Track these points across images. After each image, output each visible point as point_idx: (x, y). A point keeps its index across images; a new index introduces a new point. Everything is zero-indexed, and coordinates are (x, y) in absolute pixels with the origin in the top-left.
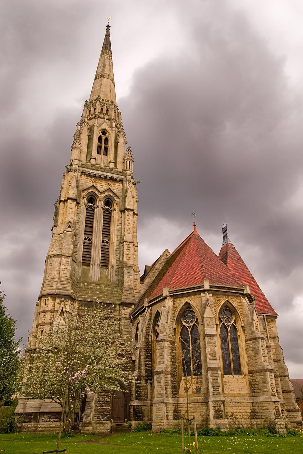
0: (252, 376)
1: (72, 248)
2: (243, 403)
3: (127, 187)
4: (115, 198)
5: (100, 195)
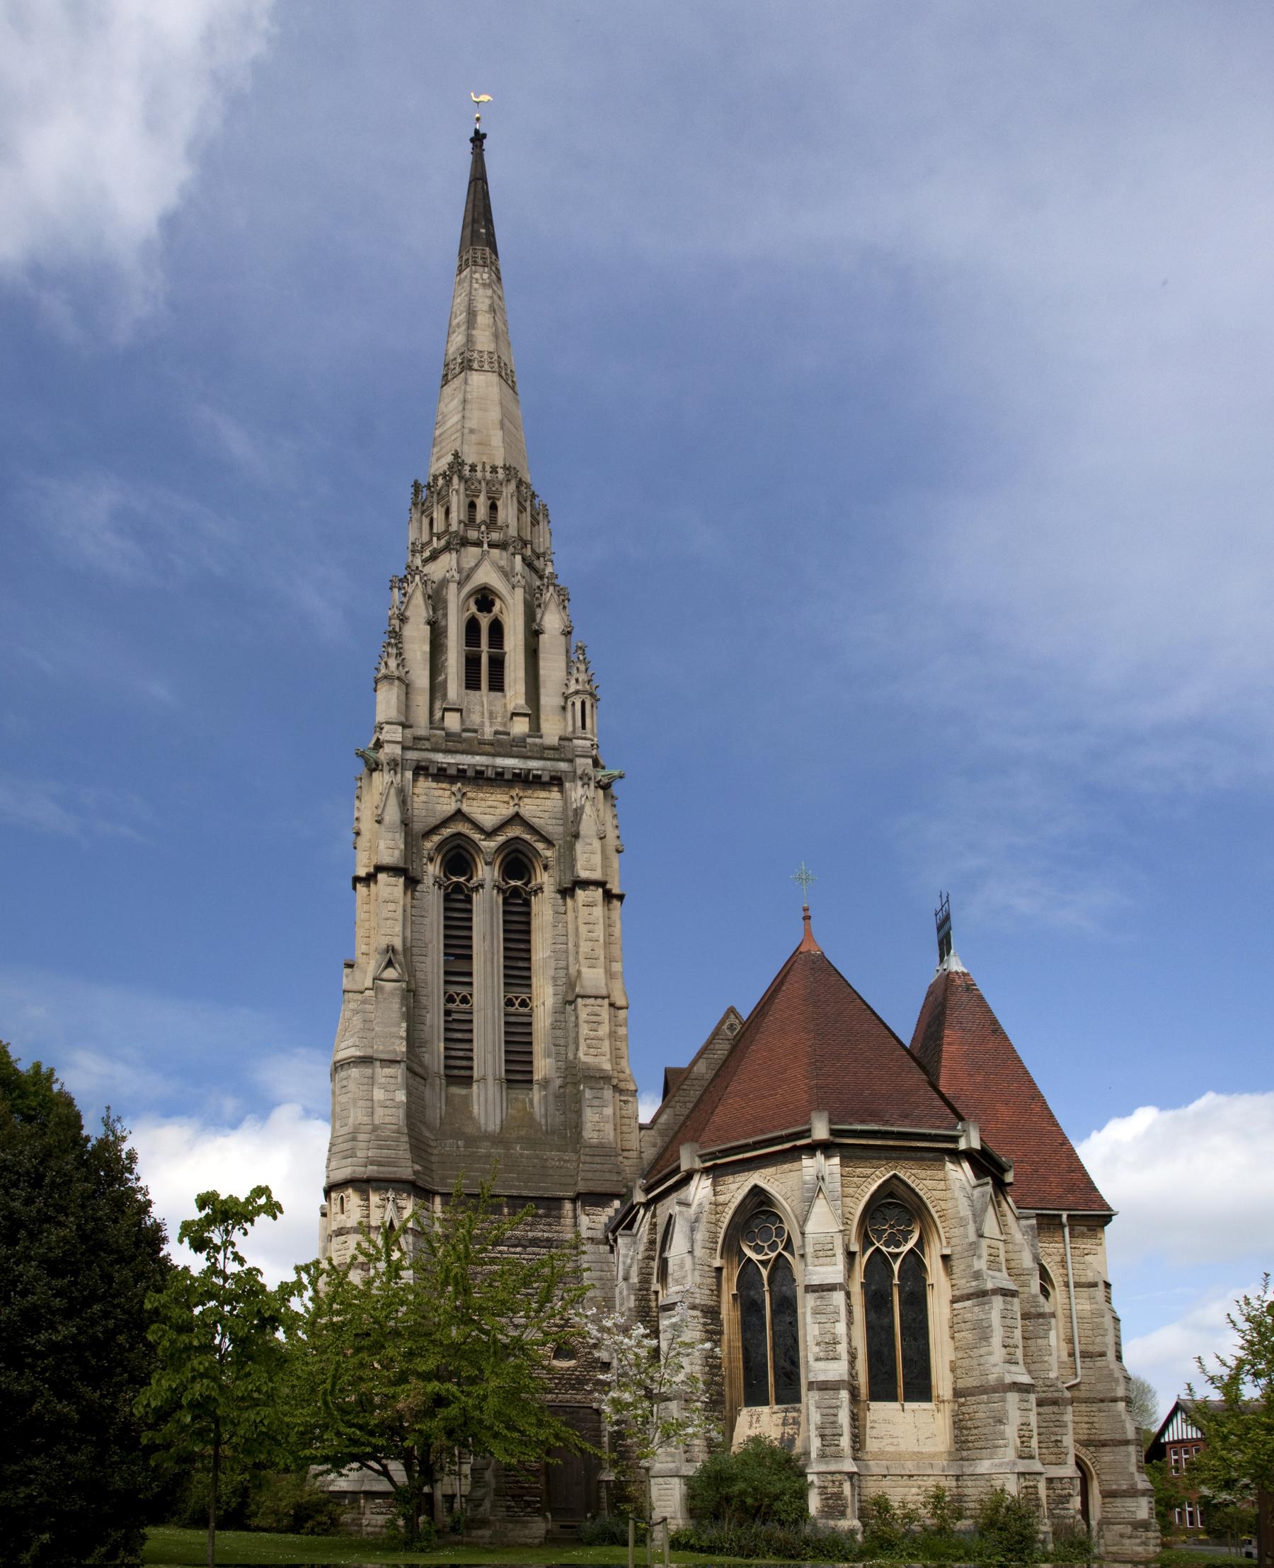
0: (963, 1405)
1: (404, 1034)
2: (925, 1478)
3: (578, 801)
4: (540, 846)
5: (484, 843)
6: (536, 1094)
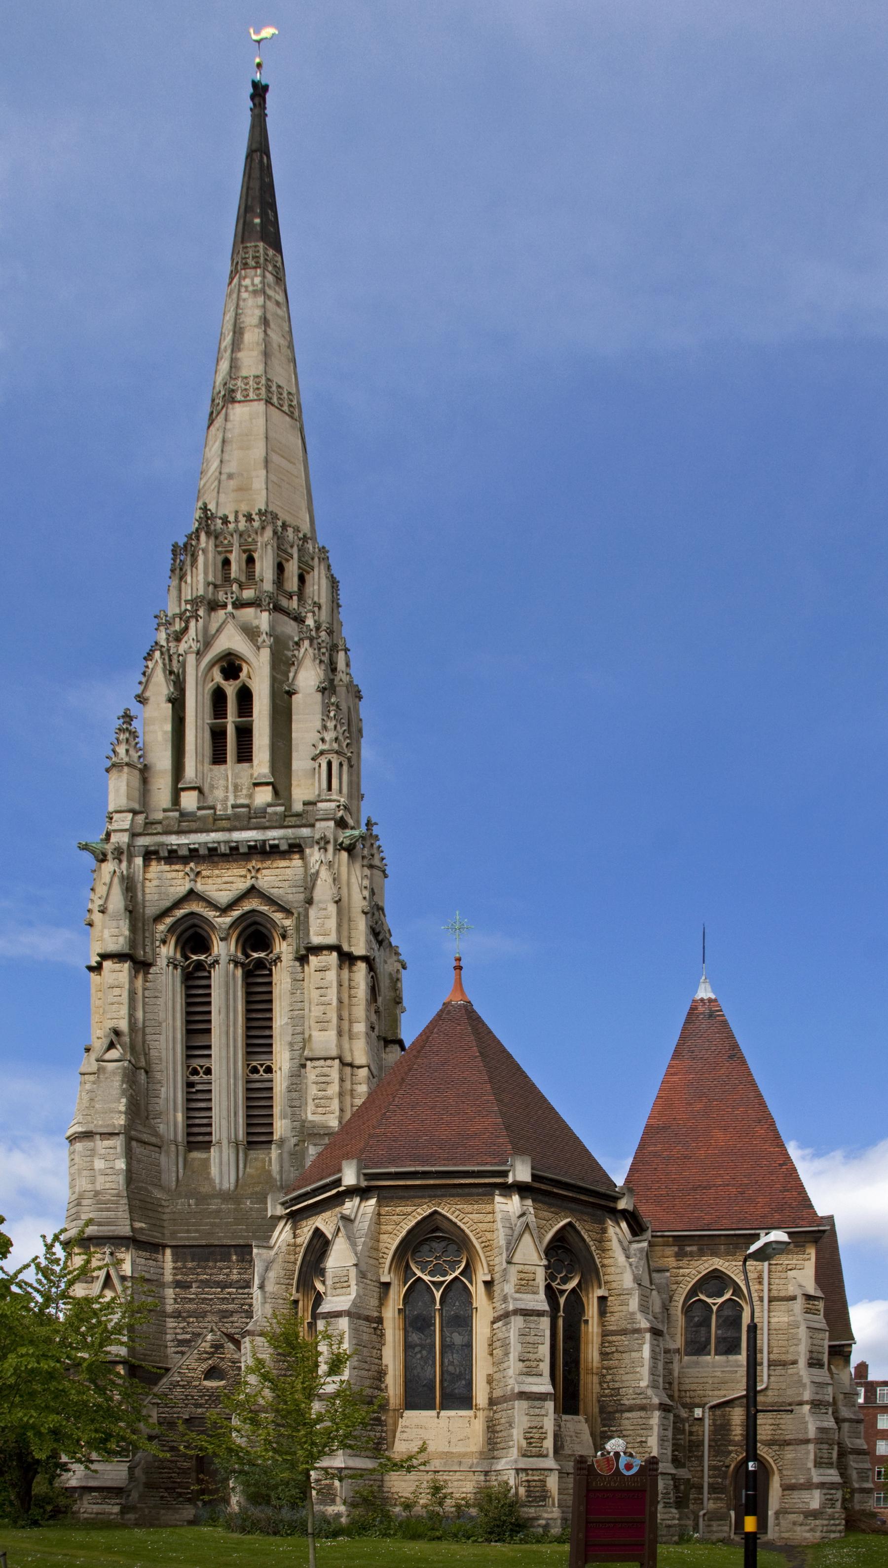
2: (451, 1473)
4: (278, 916)
5: (219, 920)
6: (274, 1152)
